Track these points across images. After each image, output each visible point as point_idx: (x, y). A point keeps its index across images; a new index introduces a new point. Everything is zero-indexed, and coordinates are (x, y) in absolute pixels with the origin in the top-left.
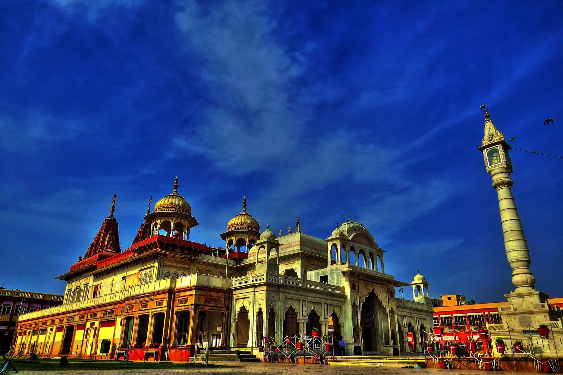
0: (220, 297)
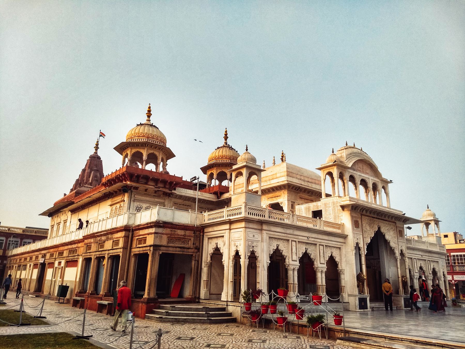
0: (189, 236)
